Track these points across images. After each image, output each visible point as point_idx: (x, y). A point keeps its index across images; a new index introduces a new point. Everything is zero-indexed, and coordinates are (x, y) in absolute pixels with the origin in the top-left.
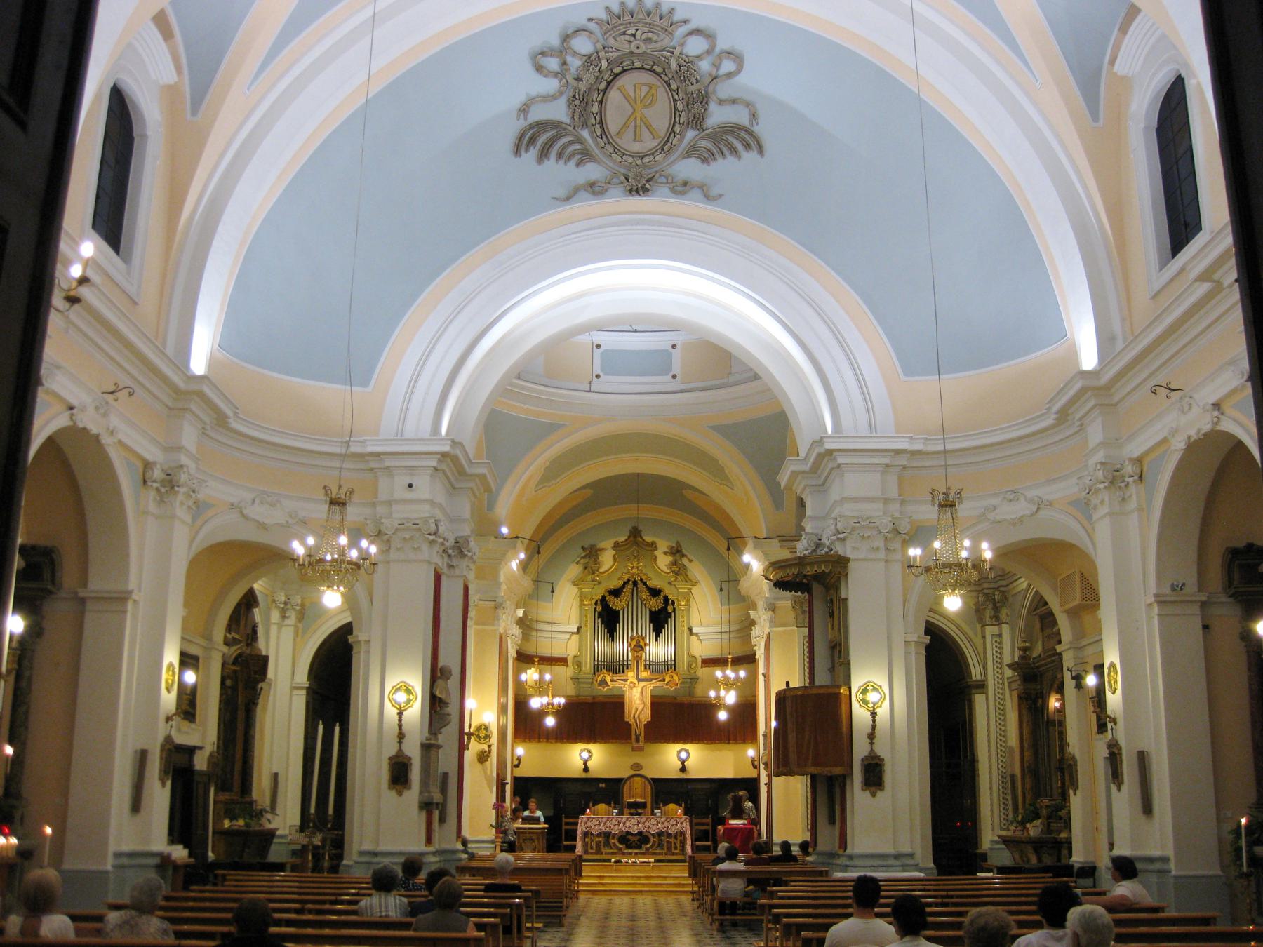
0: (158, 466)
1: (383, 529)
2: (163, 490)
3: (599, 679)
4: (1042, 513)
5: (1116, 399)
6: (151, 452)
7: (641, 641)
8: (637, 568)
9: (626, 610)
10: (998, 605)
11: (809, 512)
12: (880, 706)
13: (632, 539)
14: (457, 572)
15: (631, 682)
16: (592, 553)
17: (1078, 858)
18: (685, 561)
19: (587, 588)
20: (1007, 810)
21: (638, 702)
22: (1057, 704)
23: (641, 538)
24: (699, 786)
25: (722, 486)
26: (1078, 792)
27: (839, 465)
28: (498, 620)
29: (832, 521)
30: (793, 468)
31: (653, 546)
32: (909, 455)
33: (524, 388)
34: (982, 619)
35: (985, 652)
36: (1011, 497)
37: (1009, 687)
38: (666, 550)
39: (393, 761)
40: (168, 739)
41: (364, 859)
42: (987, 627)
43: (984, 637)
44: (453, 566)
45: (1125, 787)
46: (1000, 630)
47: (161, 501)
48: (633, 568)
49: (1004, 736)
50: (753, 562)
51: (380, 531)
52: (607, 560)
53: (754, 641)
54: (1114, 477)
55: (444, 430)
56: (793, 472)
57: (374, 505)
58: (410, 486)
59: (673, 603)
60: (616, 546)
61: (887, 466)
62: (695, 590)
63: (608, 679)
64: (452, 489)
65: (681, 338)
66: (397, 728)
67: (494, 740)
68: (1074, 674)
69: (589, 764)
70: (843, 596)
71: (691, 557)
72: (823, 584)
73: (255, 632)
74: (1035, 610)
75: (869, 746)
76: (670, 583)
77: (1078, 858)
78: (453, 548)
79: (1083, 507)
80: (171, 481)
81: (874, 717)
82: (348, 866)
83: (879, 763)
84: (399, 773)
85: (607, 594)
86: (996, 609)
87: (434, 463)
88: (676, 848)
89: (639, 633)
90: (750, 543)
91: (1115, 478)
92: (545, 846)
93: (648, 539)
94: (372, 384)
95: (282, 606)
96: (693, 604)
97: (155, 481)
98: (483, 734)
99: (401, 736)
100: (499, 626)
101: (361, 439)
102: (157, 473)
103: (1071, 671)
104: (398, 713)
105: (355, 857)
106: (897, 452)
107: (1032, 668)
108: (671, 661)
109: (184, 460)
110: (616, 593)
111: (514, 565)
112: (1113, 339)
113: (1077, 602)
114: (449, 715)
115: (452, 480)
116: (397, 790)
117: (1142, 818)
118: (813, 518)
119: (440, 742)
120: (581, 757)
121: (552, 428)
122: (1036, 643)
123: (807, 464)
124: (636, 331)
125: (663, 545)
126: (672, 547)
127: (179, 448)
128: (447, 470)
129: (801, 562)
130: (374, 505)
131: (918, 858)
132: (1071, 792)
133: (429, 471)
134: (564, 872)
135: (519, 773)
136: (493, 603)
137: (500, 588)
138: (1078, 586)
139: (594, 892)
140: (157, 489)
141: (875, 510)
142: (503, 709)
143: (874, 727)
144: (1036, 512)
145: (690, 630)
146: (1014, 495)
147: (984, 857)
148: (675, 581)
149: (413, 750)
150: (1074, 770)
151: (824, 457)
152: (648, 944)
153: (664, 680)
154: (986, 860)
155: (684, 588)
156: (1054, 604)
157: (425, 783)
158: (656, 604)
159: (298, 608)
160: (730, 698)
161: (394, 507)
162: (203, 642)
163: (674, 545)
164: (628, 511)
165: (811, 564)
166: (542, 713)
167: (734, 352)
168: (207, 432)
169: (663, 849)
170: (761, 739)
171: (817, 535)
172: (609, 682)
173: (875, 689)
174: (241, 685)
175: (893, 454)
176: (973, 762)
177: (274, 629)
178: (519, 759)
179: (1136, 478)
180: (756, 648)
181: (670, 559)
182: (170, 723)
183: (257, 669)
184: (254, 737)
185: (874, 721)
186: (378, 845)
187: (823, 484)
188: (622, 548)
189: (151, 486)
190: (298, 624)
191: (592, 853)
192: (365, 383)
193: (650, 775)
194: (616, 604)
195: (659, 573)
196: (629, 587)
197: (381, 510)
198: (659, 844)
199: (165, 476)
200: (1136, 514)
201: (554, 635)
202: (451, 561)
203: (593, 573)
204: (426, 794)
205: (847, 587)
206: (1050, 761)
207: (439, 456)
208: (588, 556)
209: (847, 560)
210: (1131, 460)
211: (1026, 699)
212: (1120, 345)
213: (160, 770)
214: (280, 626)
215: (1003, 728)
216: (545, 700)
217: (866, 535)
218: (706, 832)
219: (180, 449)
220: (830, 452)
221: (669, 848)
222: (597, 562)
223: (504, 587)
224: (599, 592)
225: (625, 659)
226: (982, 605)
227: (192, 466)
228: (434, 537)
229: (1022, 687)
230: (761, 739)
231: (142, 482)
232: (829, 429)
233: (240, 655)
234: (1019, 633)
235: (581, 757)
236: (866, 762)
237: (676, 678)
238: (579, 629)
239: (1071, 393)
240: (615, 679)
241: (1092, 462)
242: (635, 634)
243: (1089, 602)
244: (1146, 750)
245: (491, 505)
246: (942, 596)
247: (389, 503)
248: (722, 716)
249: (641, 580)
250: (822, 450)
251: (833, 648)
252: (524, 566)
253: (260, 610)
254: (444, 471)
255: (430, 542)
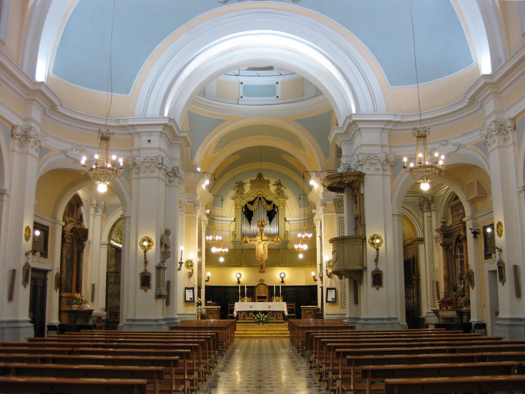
0: (19, 128)
1: (136, 162)
2: (22, 140)
3: (244, 240)
4: (460, 150)
5: (501, 90)
6: (15, 121)
7: (263, 222)
8: (261, 192)
9: (256, 210)
10: (430, 202)
11: (344, 153)
12: (381, 246)
13: (258, 178)
14: (173, 184)
15: (259, 242)
16: (240, 185)
17: (474, 319)
18: (282, 188)
19: (238, 201)
20: (434, 298)
21: (262, 250)
22: (192, 357)
23: (263, 177)
24: (289, 289)
25: (300, 150)
26: (474, 288)
27: (359, 128)
28: (196, 211)
29: (356, 156)
30: (336, 132)
31: (268, 182)
32: (393, 124)
33: (206, 102)
34: (422, 209)
35: (424, 225)
36: (444, 143)
37: (435, 240)
38: (274, 183)
39: (143, 275)
40: (27, 265)
41: (130, 323)
42: (425, 213)
43: (423, 218)
44: (171, 181)
45: (507, 284)
46: (431, 214)
47: (21, 146)
48: (259, 191)
49: (433, 264)
50: (315, 184)
51: (135, 163)
52: (247, 188)
53: (315, 222)
54: (500, 129)
55: (166, 114)
56: (336, 134)
57: (131, 151)
58: (149, 141)
59: (277, 207)
60: (251, 182)
61: (383, 129)
62: (287, 201)
63: (248, 240)
64: (171, 144)
65: (281, 79)
66: (144, 259)
67: (195, 267)
68: (473, 231)
69: (240, 280)
70: (362, 192)
71: (285, 186)
72: (351, 188)
73: (81, 217)
74: (448, 204)
75: (375, 265)
76: (276, 198)
77: (474, 319)
78: (171, 172)
79: (483, 146)
80: (26, 135)
81: (378, 251)
82: (122, 326)
83: (381, 274)
84: (145, 281)
85: (247, 204)
86: (429, 204)
87: (161, 130)
88: (280, 317)
89: (262, 219)
90: (313, 175)
91: (501, 129)
92: (219, 316)
93: (266, 178)
94: (130, 93)
95: (95, 206)
96: (286, 207)
97: (17, 135)
98: (189, 264)
99: (146, 263)
100: (196, 214)
101: (125, 118)
102: (18, 131)
103: (471, 229)
104: (144, 252)
105: (125, 322)
106: (388, 122)
107: (447, 231)
108: (277, 233)
109: (33, 125)
110: (252, 203)
111: (204, 186)
112: (500, 60)
113: (475, 195)
114: (169, 252)
115: (171, 140)
116: (144, 290)
117: (515, 298)
118: (345, 156)
119: (166, 266)
120: (236, 277)
121: (220, 122)
122: (449, 219)
123: (343, 130)
124: (259, 76)
125: (273, 181)
126: (277, 182)
127: (30, 119)
128: (167, 134)
129: (341, 175)
130: (131, 151)
131: (399, 320)
132: (471, 288)
133: (159, 134)
134: (224, 328)
135: (208, 284)
136: (194, 203)
137: (197, 197)
138: (476, 188)
139: (242, 337)
140: (19, 139)
141: (377, 150)
142: (200, 254)
143: (378, 256)
144: (457, 150)
145: (285, 219)
146: (446, 142)
147: (423, 319)
148: (278, 197)
149: (152, 270)
150: (472, 277)
151: (352, 125)
152: (271, 391)
153: (274, 240)
154: (424, 321)
155: (282, 201)
156: (462, 198)
157: (158, 285)
158: (270, 208)
159: (103, 207)
160: (305, 247)
161: (142, 152)
162: (52, 220)
163: (278, 181)
164: (256, 166)
165: (346, 176)
166: (218, 255)
167: (306, 77)
168: (46, 113)
169: (274, 317)
170: (318, 266)
171: (348, 164)
172: (248, 242)
173: (378, 238)
174: (75, 243)
175: (385, 123)
176: (418, 275)
177: (91, 217)
178: (208, 278)
179: (512, 128)
180: (316, 225)
181: (276, 187)
182: (28, 256)
183: (82, 235)
184: (82, 267)
185: (378, 253)
186: (135, 315)
187: (351, 140)
188: (255, 182)
189: (16, 137)
190: (103, 215)
191: (241, 320)
192: (127, 92)
193: (268, 285)
194: (252, 208)
195: (271, 194)
196: (258, 200)
197: (135, 153)
198: (272, 315)
199: (23, 133)
200: (512, 147)
201: (223, 222)
202: (170, 178)
203: (241, 194)
204: (159, 291)
205: (364, 188)
206: (456, 275)
207: (163, 126)
208: (239, 186)
209: (364, 174)
210: (510, 119)
211: (444, 245)
212: (503, 62)
213: (23, 280)
214: (95, 216)
215: (432, 260)
216: (219, 250)
217: (373, 162)
218: (293, 309)
219: (30, 119)
220: (355, 122)
221: (277, 317)
222: (243, 190)
223: (199, 197)
224: (244, 203)
225: (256, 232)
226: (422, 202)
227: (38, 129)
228: (161, 166)
229: (442, 240)
230: (318, 266)
231: (11, 135)
232: (354, 111)
233: (74, 228)
234: (441, 215)
235: (236, 277)
236: (374, 273)
237: (279, 239)
238: (235, 219)
239: (478, 87)
240: (251, 240)
241: (488, 122)
242: (260, 220)
243: (481, 195)
244: (517, 265)
245: (192, 158)
246: (420, 183)
247: (139, 150)
248: (301, 256)
249: (263, 197)
250: (351, 121)
251: (357, 218)
252: (210, 188)
253: (84, 207)
254: (165, 134)
255: (159, 168)
